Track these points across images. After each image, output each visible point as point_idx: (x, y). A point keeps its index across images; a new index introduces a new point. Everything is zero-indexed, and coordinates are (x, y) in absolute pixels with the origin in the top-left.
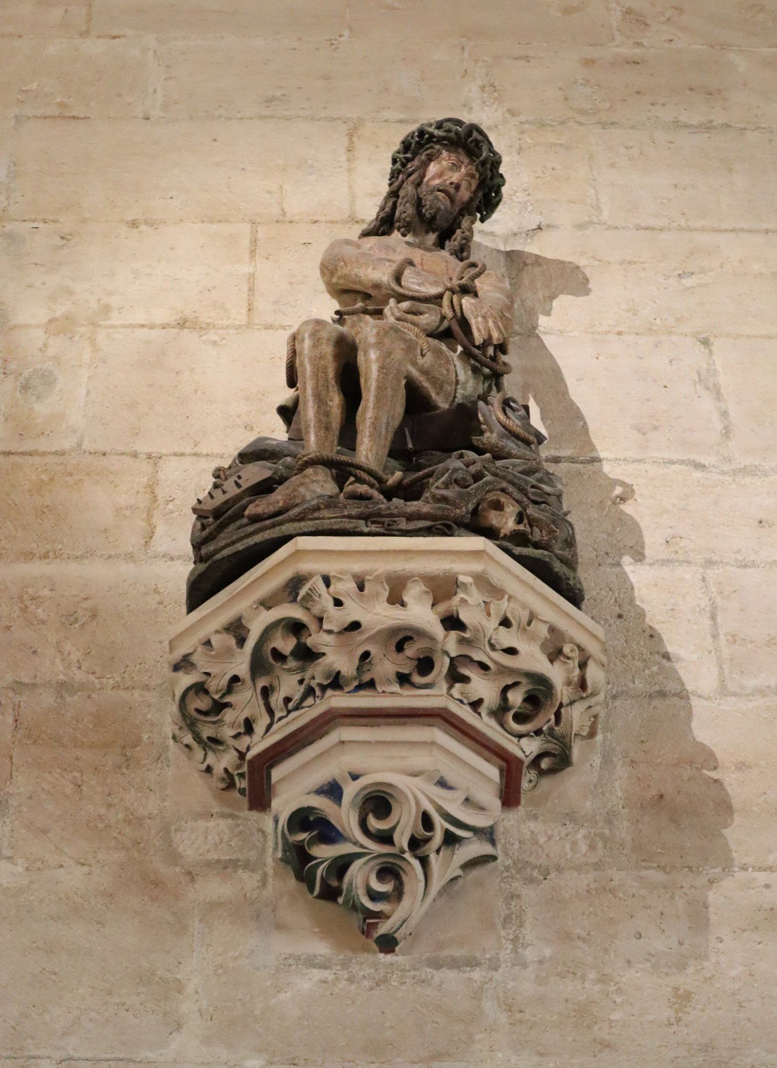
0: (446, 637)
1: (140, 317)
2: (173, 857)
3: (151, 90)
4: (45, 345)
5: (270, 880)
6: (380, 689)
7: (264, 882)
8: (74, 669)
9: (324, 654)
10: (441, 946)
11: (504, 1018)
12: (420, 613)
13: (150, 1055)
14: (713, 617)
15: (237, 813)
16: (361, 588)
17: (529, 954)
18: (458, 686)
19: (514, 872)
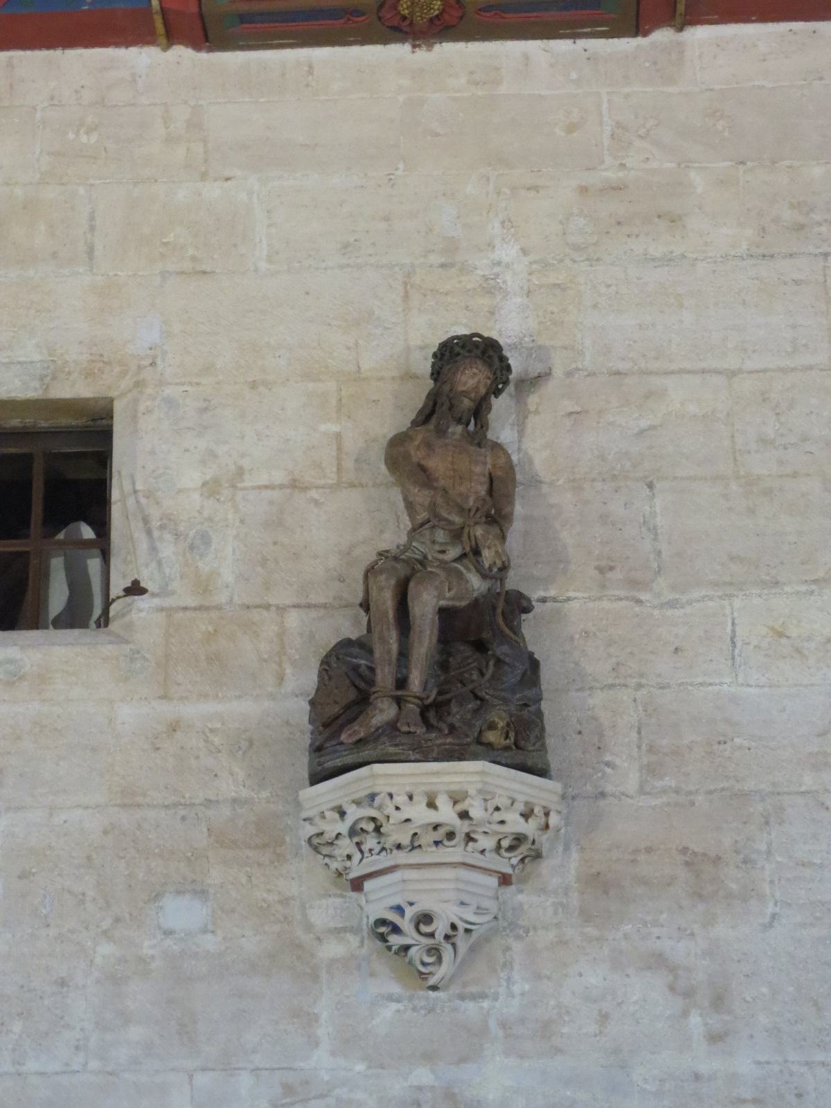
0: (462, 825)
1: (263, 479)
2: (309, 927)
3: (258, 240)
4: (202, 507)
5: (366, 942)
6: (424, 849)
7: (362, 943)
8: (241, 787)
9: (391, 835)
10: (465, 985)
11: (501, 1033)
12: (446, 813)
13: (302, 1064)
14: (639, 732)
15: (345, 894)
16: (411, 798)
17: (516, 989)
18: (471, 844)
19: (508, 931)
